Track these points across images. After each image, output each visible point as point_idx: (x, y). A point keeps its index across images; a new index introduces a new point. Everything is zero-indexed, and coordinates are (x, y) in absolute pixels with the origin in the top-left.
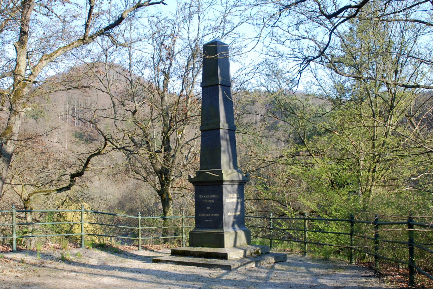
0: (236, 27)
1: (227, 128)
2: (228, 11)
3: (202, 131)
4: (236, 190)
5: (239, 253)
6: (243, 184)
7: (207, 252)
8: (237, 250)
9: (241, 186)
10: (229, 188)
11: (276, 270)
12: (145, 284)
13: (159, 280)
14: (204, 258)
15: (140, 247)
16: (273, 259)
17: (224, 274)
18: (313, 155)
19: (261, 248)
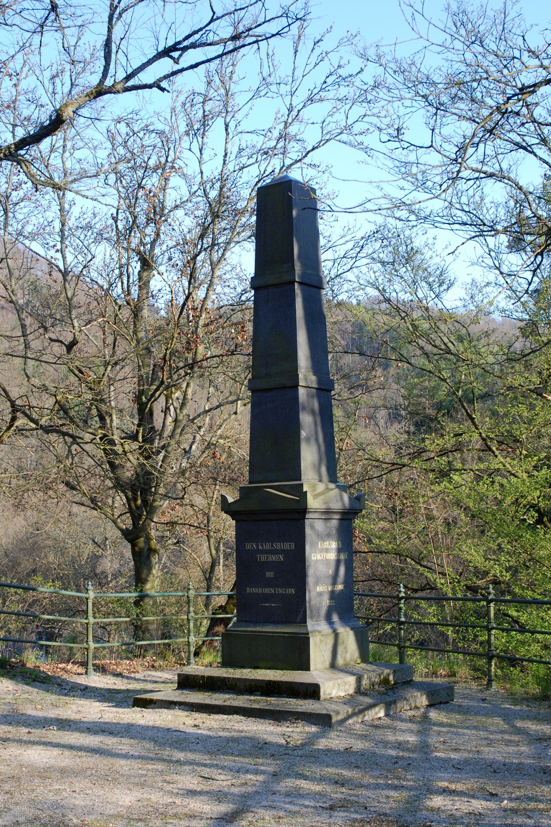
0: (313, 149)
1: (315, 385)
2: (294, 113)
3: (253, 392)
4: (334, 532)
5: (345, 683)
6: (350, 517)
7: (270, 681)
8: (341, 675)
9: (346, 522)
10: (320, 525)
11: (435, 724)
12: (136, 764)
13: (166, 752)
14: (262, 695)
15: (90, 666)
16: (424, 696)
17: (316, 737)
18: (494, 449)
19: (395, 672)
